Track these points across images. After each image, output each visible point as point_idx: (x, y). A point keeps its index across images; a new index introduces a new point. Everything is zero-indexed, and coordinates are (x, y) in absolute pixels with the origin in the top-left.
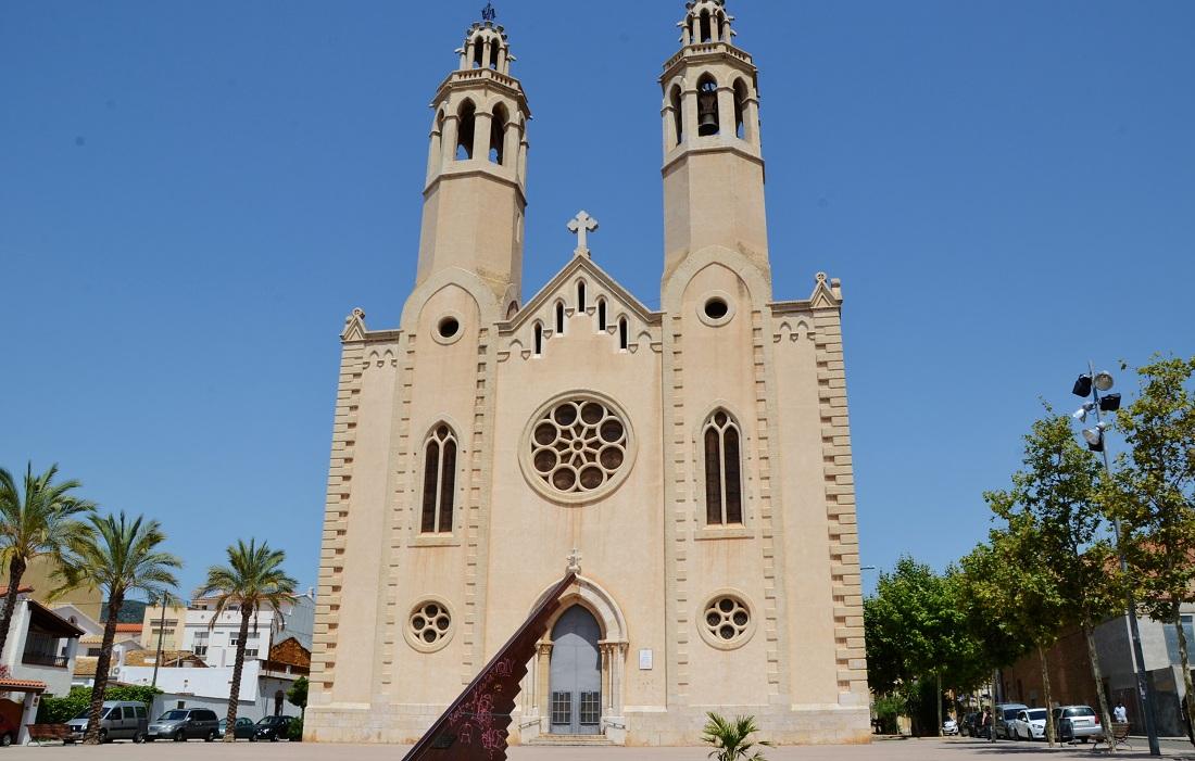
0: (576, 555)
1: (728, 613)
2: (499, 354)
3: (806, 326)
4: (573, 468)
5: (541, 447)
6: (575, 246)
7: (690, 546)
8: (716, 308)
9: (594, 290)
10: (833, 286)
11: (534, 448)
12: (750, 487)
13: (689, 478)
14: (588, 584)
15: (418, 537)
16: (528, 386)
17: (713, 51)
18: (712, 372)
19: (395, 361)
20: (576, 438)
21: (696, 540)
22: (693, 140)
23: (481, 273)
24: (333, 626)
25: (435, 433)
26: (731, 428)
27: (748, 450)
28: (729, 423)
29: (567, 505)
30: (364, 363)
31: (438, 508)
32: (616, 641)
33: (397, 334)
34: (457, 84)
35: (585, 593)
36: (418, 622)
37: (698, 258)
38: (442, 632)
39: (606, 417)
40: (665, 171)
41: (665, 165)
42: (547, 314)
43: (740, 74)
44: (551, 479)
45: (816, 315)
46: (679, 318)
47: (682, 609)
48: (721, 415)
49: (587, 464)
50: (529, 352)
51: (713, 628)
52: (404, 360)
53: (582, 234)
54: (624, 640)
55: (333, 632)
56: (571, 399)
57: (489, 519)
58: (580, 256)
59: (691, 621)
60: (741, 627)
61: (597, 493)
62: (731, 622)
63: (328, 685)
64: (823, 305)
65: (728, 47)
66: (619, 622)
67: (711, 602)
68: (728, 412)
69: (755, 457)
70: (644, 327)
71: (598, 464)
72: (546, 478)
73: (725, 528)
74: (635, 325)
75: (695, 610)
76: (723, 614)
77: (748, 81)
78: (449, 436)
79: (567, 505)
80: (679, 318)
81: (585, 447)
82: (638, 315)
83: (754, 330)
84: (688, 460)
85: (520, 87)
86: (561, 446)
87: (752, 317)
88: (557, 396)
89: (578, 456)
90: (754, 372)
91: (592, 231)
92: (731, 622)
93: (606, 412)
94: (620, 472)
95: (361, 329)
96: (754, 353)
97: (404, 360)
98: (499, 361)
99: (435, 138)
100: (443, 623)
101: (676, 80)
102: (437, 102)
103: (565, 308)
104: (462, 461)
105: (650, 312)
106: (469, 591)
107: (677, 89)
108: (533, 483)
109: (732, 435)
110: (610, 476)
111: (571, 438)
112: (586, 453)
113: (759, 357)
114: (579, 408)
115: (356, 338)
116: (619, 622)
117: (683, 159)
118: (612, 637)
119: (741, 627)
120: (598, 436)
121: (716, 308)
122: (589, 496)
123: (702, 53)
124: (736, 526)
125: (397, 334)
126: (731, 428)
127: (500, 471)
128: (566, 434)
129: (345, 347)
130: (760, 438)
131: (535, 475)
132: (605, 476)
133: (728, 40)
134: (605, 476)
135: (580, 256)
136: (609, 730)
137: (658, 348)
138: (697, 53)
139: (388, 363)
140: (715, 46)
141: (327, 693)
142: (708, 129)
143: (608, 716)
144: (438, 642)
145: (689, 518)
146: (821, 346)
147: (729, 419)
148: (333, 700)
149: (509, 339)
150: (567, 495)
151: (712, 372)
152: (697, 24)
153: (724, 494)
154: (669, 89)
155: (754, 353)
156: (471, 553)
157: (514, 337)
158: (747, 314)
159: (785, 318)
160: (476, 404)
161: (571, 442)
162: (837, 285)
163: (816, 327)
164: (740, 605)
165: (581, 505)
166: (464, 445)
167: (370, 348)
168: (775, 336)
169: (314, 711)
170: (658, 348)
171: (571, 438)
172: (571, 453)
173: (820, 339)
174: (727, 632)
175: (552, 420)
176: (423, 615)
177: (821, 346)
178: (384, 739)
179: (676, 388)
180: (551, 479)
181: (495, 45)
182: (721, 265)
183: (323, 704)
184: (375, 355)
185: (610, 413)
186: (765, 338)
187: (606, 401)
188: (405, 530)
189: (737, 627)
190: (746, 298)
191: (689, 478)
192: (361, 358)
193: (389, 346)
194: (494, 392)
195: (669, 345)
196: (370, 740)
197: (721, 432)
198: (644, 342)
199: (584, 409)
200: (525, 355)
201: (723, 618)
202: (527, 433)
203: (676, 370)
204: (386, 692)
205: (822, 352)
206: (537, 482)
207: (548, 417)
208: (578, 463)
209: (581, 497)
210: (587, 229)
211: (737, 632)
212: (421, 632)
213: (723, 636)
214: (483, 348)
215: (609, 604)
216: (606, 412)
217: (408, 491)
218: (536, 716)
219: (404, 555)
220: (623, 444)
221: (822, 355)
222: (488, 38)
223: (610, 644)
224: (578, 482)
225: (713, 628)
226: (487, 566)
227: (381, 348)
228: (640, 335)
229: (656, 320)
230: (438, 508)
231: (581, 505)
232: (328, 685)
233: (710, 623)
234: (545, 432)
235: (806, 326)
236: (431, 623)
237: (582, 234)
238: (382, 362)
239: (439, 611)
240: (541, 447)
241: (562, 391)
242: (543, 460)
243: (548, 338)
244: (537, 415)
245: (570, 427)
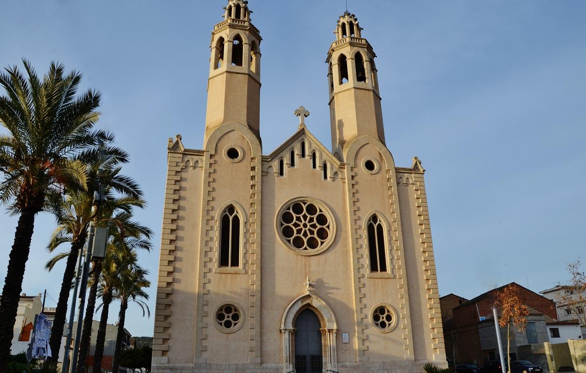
56: (301, 201)
92: (385, 316)
100: (236, 317)
153: (377, 262)
174: (228, 325)
204: (205, 355)
212: (233, 322)
236: (228, 317)
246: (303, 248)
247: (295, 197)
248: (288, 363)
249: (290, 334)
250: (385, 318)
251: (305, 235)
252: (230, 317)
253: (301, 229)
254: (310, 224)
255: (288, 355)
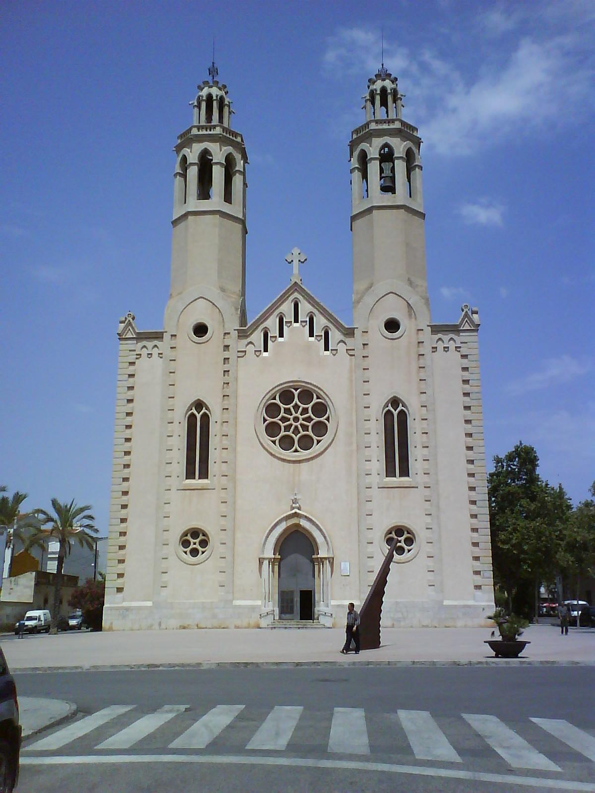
0: (298, 497)
1: (195, 540)
2: (238, 351)
3: (455, 341)
4: (293, 435)
5: (270, 420)
6: (292, 274)
7: (375, 492)
8: (392, 325)
9: (305, 308)
10: (473, 313)
11: (265, 420)
12: (415, 453)
13: (374, 446)
14: (306, 517)
15: (384, 480)
16: (261, 375)
17: (392, 126)
18: (390, 371)
19: (162, 354)
20: (294, 415)
21: (379, 488)
22: (378, 198)
23: (223, 290)
24: (122, 547)
25: (194, 408)
26: (402, 411)
27: (414, 427)
28: (400, 408)
29: (289, 461)
30: (137, 355)
31: (197, 462)
32: (326, 556)
33: (162, 333)
34: (196, 136)
35: (303, 523)
36: (185, 544)
37: (381, 288)
38: (204, 550)
39: (315, 400)
40: (175, 223)
41: (174, 219)
42: (272, 323)
43: (230, 149)
44: (277, 442)
45: (461, 334)
46: (367, 332)
47: (370, 535)
48: (395, 402)
49: (302, 433)
50: (261, 351)
51: (185, 550)
52: (169, 353)
53: (296, 263)
54: (331, 555)
55: (122, 552)
56: (290, 387)
57: (235, 471)
58: (296, 282)
59: (376, 542)
60: (410, 548)
61: (310, 454)
62: (197, 546)
63: (120, 590)
64: (467, 327)
65: (224, 129)
66: (327, 543)
67: (389, 530)
68: (400, 400)
69: (419, 432)
70: (342, 337)
71: (310, 433)
72: (274, 442)
73: (397, 480)
74: (335, 335)
75: (175, 536)
76: (192, 541)
77: (238, 156)
78: (204, 410)
79: (289, 461)
80: (367, 332)
81: (301, 421)
82: (337, 328)
83: (419, 343)
84: (373, 433)
85: (242, 140)
86: (284, 419)
87: (417, 334)
88: (281, 384)
89: (296, 427)
90: (418, 372)
91: (303, 262)
92: (197, 546)
93: (315, 397)
94: (326, 440)
95: (133, 328)
96: (419, 359)
97: (169, 353)
98: (238, 357)
99: (179, 179)
100: (204, 543)
101: (364, 146)
102: (179, 148)
103: (284, 320)
104: (214, 429)
105: (347, 327)
106: (223, 521)
107: (184, 158)
108: (266, 446)
109: (403, 416)
110: (319, 442)
111: (303, 420)
112: (302, 425)
113: (422, 362)
114: (296, 393)
115: (129, 335)
116: (327, 543)
117: (370, 210)
118: (322, 554)
119: (410, 548)
120: (310, 414)
121: (392, 325)
122: (305, 455)
123: (385, 126)
124: (406, 479)
125: (162, 333)
126: (205, 414)
127: (242, 439)
128: (287, 411)
129: (122, 342)
130: (422, 419)
131: (267, 440)
132: (315, 442)
133: (226, 125)
134: (315, 442)
135: (296, 282)
136: (321, 618)
137: (351, 353)
138: (380, 127)
139: (155, 355)
140: (214, 127)
141: (120, 595)
142: (389, 188)
143: (320, 607)
144: (200, 557)
145: (374, 473)
146: (464, 356)
147: (401, 405)
148: (124, 600)
149: (246, 341)
150: (289, 454)
151: (390, 371)
152: (204, 105)
153: (397, 458)
154: (356, 154)
155: (419, 359)
156: (223, 494)
157: (249, 340)
158: (414, 331)
159: (440, 336)
160: (223, 388)
161: (291, 417)
162: (476, 313)
163: (461, 343)
164: (204, 535)
165: (299, 462)
166: (215, 417)
167: (140, 345)
168: (433, 348)
169: (111, 609)
170: (351, 353)
171: (296, 413)
172: (291, 425)
173: (464, 351)
174: (194, 553)
175: (277, 401)
176: (189, 538)
177: (464, 356)
178: (163, 626)
179: (364, 382)
180: (277, 442)
181: (221, 100)
182: (396, 294)
183: (116, 604)
184: (145, 349)
185: (318, 398)
186: (426, 349)
187: (316, 389)
188: (174, 477)
189: (201, 549)
190: (413, 320)
191: (374, 446)
192: (135, 350)
193: (156, 342)
194: (236, 379)
195: (359, 352)
196: (154, 627)
197: (395, 413)
198: (342, 348)
199: (299, 394)
200: (258, 353)
201: (192, 543)
202: (260, 410)
203: (364, 369)
204: (164, 592)
205: (465, 361)
206: (268, 445)
207: (274, 399)
208: (297, 432)
209: (299, 456)
210: (299, 261)
211: (406, 551)
212: (188, 550)
213: (192, 555)
214: (227, 347)
215: (321, 530)
216: (315, 397)
217: (175, 449)
218: (271, 608)
219: (175, 496)
220: (328, 419)
221: (465, 363)
222: (217, 96)
223: (321, 558)
224: (296, 445)
225: (185, 550)
226: (234, 503)
227: (149, 344)
228: (153, 348)
229: (350, 332)
230: (197, 462)
231: (299, 462)
232: (120, 590)
233: (183, 546)
234: (272, 410)
235: (455, 341)
236: (195, 544)
237: (296, 263)
238: (151, 354)
239: (406, 532)
240: (270, 420)
241: (284, 381)
242: (272, 429)
243: (273, 342)
244: (267, 397)
245: (290, 406)
246: (299, 390)
247: (282, 382)
248: (267, 601)
249: (270, 563)
250: (195, 546)
251: (296, 407)
252: (197, 544)
253: (289, 420)
254: (299, 426)
255: (267, 591)
